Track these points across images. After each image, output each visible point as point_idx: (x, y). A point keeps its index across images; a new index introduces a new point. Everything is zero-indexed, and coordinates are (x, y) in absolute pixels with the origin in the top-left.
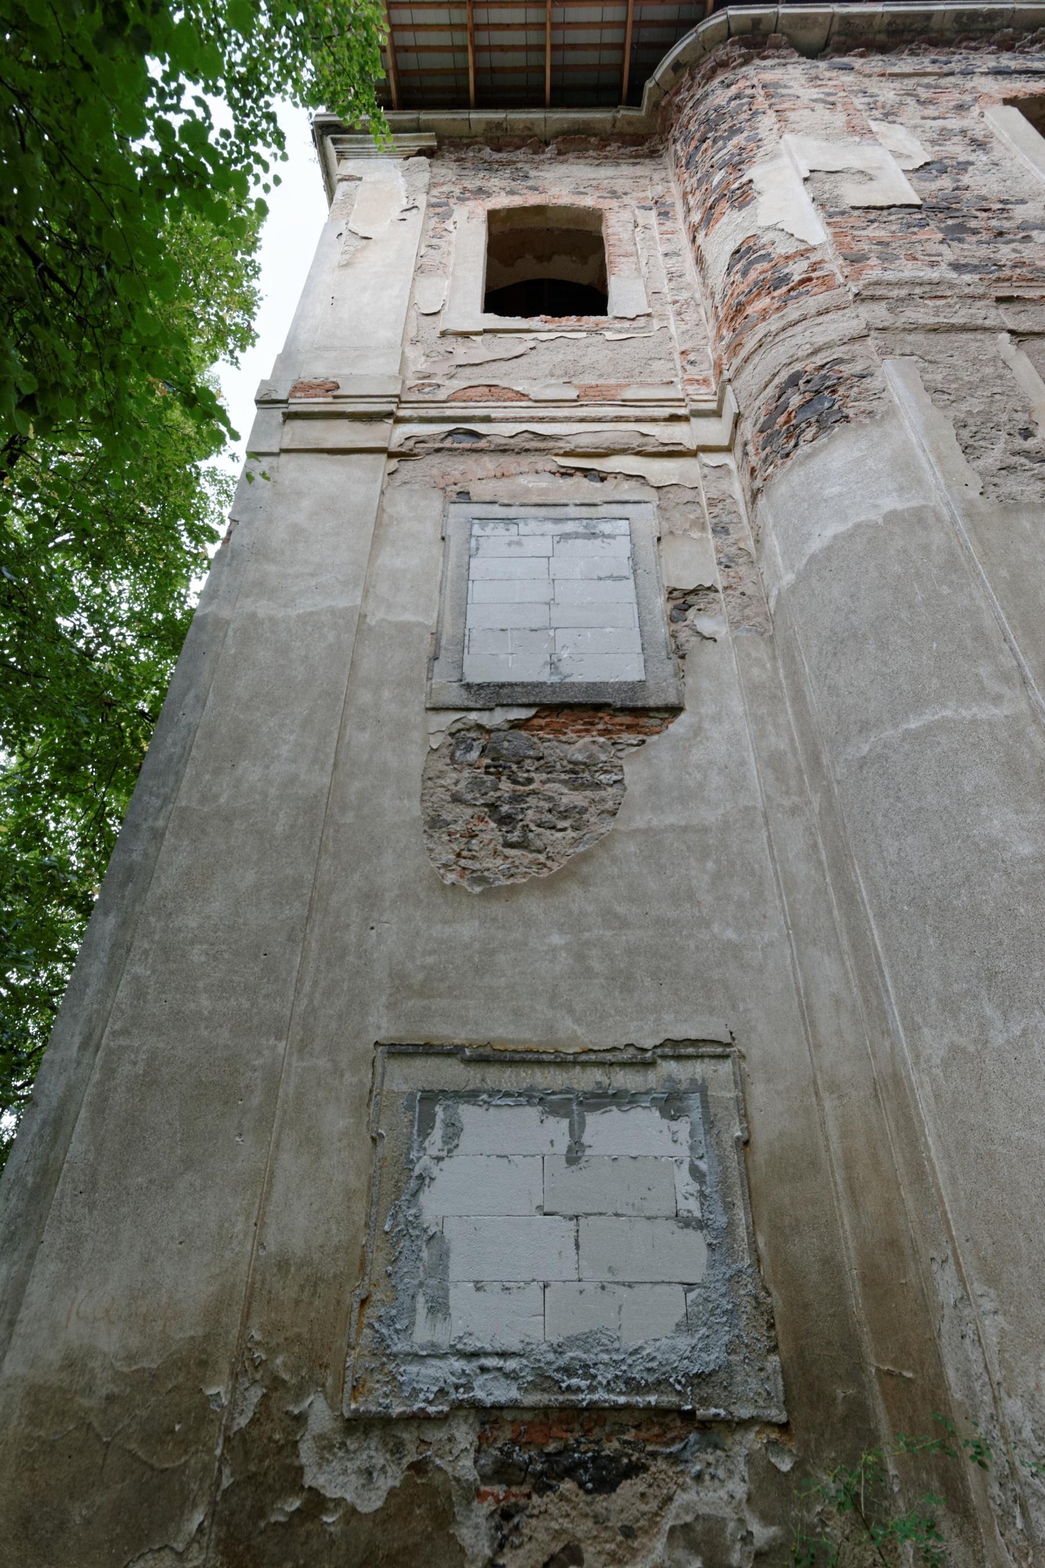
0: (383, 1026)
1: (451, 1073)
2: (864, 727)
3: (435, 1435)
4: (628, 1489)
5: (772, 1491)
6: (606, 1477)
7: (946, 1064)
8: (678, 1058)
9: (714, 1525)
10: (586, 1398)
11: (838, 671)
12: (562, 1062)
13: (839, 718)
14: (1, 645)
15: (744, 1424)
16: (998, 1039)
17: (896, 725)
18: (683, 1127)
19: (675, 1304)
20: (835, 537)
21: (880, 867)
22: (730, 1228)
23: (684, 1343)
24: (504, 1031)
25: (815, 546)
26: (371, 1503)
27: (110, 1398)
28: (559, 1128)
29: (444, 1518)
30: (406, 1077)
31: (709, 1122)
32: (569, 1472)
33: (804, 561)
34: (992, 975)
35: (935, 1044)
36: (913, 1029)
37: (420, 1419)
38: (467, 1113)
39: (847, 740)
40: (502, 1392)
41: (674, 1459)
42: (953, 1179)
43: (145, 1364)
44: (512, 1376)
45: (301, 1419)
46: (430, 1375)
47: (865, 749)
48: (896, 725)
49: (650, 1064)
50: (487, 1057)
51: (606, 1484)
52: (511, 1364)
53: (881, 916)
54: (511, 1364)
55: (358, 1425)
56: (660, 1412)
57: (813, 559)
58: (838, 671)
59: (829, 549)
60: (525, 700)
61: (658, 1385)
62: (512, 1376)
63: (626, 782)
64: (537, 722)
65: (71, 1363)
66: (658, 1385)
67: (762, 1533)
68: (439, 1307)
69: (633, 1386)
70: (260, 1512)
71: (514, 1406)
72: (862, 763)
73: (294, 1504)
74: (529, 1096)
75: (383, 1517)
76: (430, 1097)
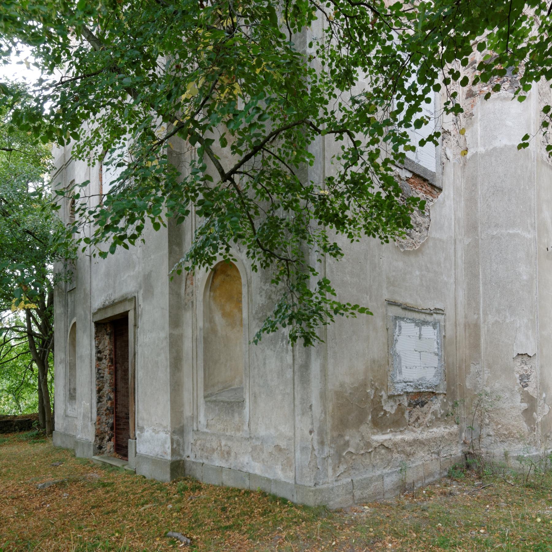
0: (386, 296)
1: (398, 311)
2: (497, 226)
3: (401, 398)
4: (426, 406)
5: (444, 405)
6: (423, 404)
7: (493, 324)
8: (437, 313)
9: (436, 411)
10: (422, 390)
11: (493, 201)
12: (419, 312)
13: (488, 218)
14: (177, 2)
15: (440, 394)
16: (508, 321)
17: (506, 230)
18: (436, 331)
19: (433, 371)
20: (505, 145)
21: (489, 271)
22: (441, 356)
23: (435, 379)
24: (409, 301)
25: (498, 144)
26: (393, 412)
27: (350, 393)
28: (417, 329)
29: (403, 413)
30: (394, 311)
31: (440, 331)
32: (418, 404)
33: (491, 147)
34: (511, 306)
35: (491, 319)
36: (485, 314)
37: (399, 395)
38: (403, 323)
39: (489, 227)
40: (410, 390)
41: (431, 401)
42: (486, 348)
43: (355, 385)
44: (411, 386)
45: (381, 396)
46: (400, 386)
47: (495, 233)
48: (506, 230)
49: (432, 314)
50: (406, 308)
51: (423, 406)
52: (412, 384)
53: (485, 284)
54: (412, 384)
55: (390, 397)
56: (430, 392)
57: (495, 149)
58: (493, 201)
59: (502, 149)
60: (410, 169)
61: (431, 387)
62: (411, 386)
63: (431, 217)
64: (412, 180)
65: (342, 385)
66: (431, 387)
67: (442, 412)
68: (400, 372)
69: (428, 388)
70: (377, 415)
71: (413, 392)
72: (493, 237)
73: (382, 413)
74: (413, 320)
75: (395, 414)
76: (396, 318)
